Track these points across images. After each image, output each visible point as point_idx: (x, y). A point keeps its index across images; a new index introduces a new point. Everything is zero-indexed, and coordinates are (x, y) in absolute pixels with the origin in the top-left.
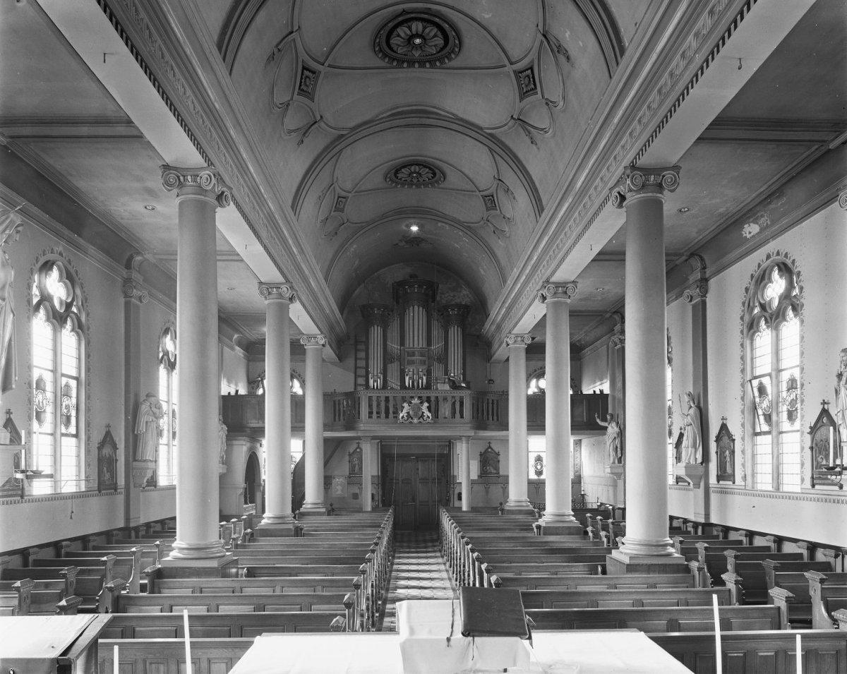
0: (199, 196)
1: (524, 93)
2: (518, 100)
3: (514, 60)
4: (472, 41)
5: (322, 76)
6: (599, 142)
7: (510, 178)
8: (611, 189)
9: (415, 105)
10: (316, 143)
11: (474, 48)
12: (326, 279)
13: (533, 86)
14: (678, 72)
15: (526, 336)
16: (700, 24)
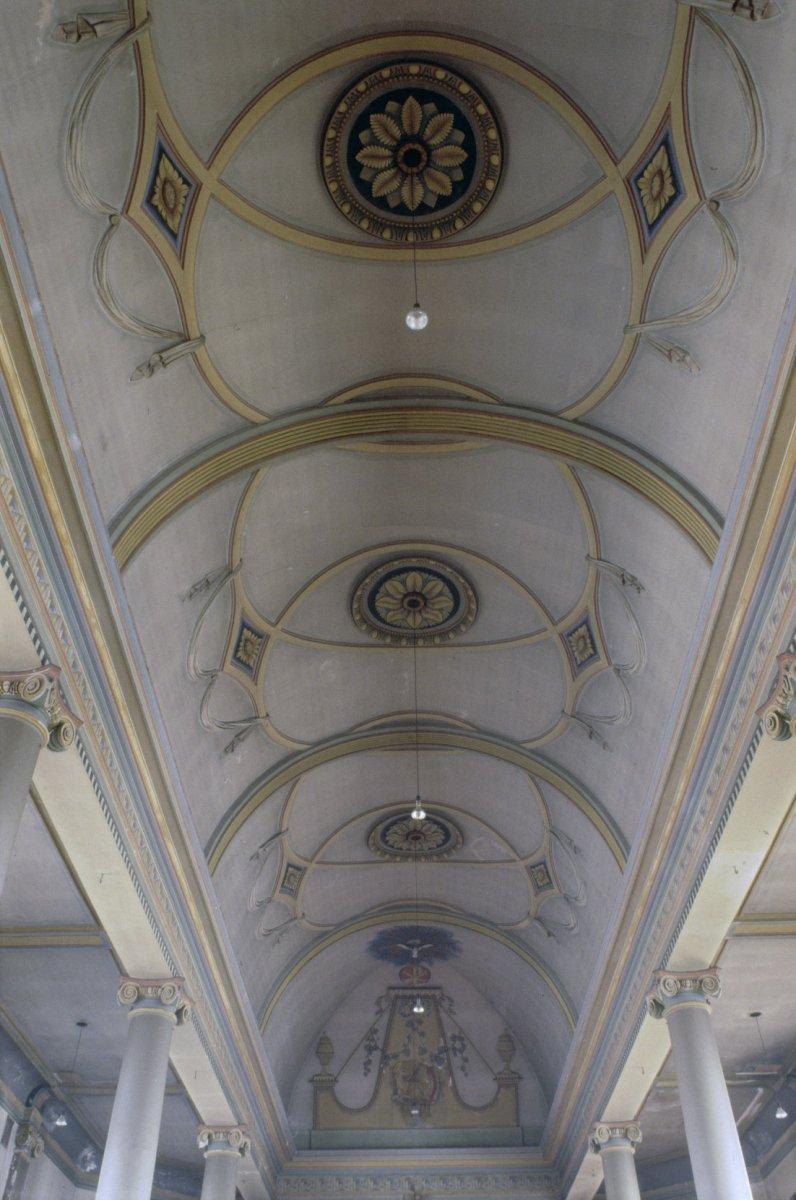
0: (149, 1010)
1: (579, 666)
2: (569, 678)
3: (522, 855)
4: (495, 590)
5: (270, 644)
6: (701, 706)
7: (573, 821)
8: (760, 711)
9: (401, 803)
10: (247, 762)
11: (479, 843)
12: (260, 1017)
13: (591, 651)
14: (781, 611)
15: (631, 1127)
16: (775, 603)
